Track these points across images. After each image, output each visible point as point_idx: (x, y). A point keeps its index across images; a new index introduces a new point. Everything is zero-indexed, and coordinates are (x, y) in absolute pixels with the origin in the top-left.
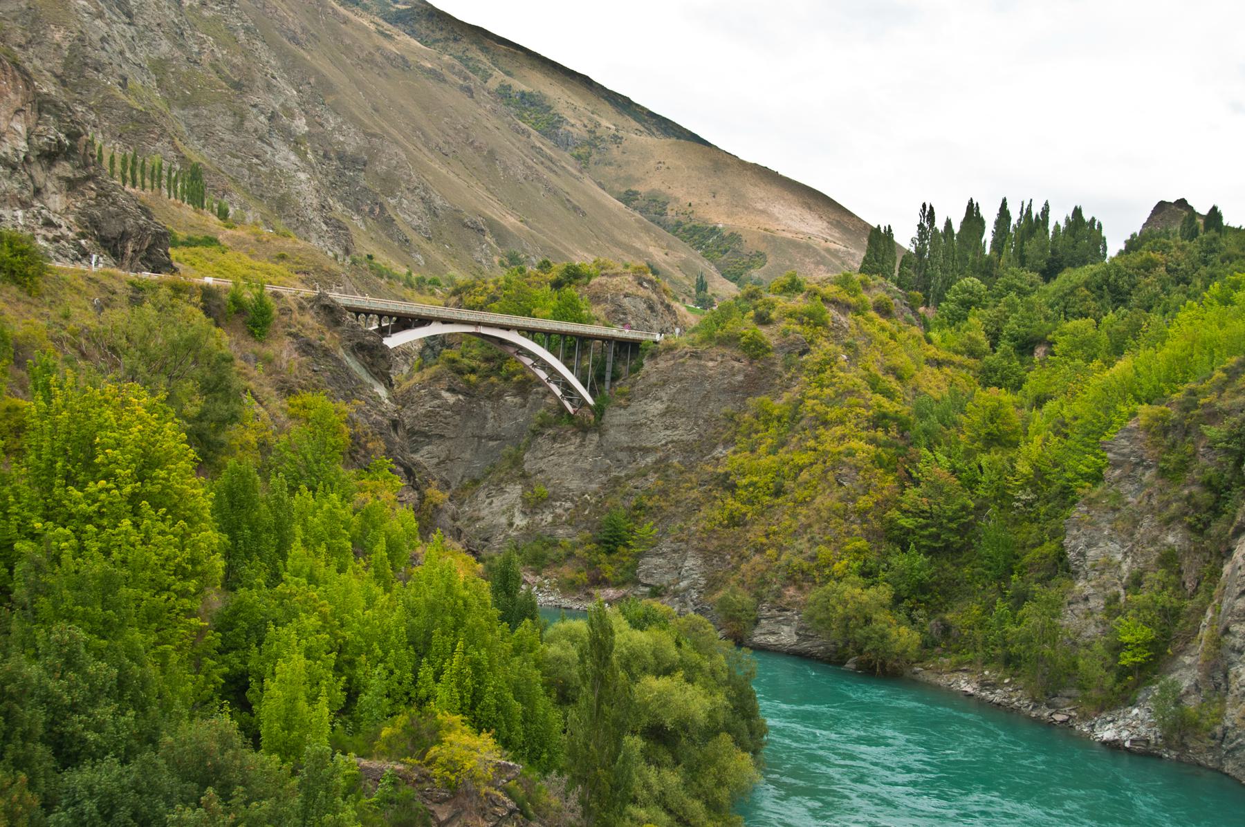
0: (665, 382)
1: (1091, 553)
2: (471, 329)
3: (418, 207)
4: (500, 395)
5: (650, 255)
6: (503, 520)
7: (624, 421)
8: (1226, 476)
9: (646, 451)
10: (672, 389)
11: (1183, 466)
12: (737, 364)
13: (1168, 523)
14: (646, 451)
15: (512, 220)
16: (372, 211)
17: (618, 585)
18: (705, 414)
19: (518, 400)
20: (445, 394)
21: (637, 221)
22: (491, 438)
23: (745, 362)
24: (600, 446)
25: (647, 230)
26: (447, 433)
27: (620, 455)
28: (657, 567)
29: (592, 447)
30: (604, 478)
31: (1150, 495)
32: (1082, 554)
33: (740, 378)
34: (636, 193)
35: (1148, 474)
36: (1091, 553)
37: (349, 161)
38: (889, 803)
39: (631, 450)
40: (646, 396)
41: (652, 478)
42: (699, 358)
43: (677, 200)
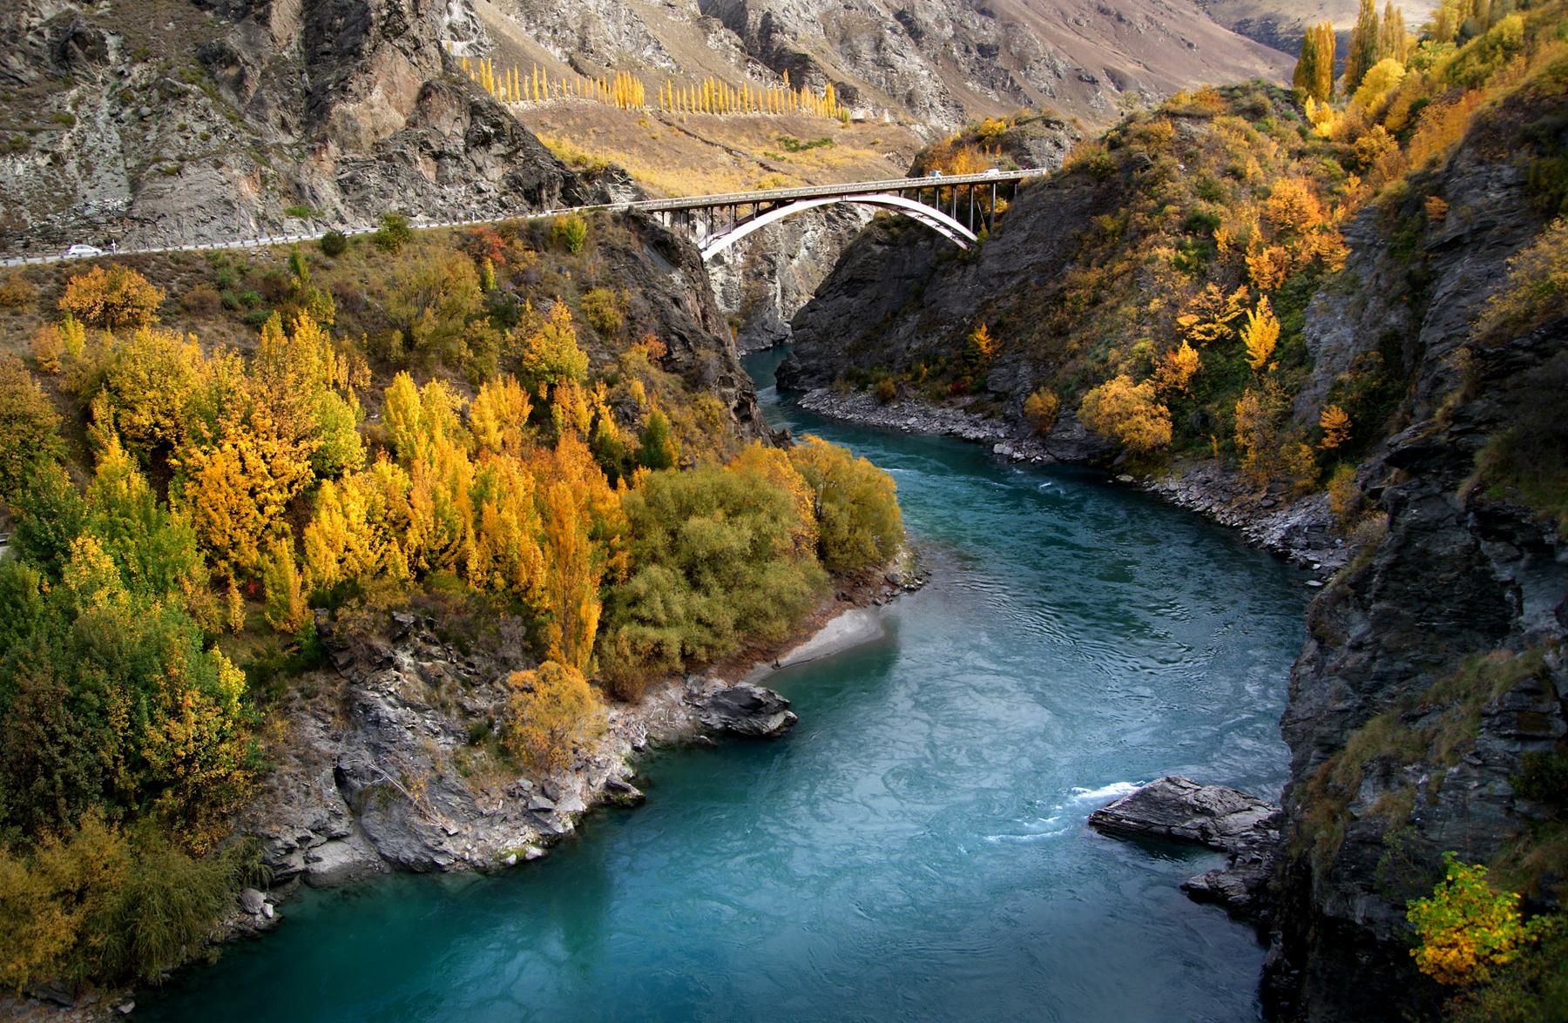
0: (1027, 213)
1: (1325, 339)
2: (838, 200)
3: (1048, 73)
4: (915, 242)
5: (1256, 72)
6: (904, 345)
7: (997, 250)
8: (1266, 270)
9: (1012, 275)
10: (1033, 218)
11: (1410, 244)
12: (1087, 188)
13: (1391, 304)
14: (1012, 275)
15: (1132, 66)
16: (1004, 85)
17: (973, 393)
18: (1058, 237)
19: (927, 243)
20: (874, 247)
21: (1246, 45)
22: (907, 278)
23: (1094, 185)
24: (976, 276)
25: (1255, 51)
26: (876, 278)
27: (992, 281)
28: (1001, 376)
29: (970, 277)
30: (979, 302)
31: (1378, 277)
32: (1317, 341)
33: (1089, 200)
34: (1248, 21)
35: (1381, 254)
36: (1325, 339)
37: (985, 51)
38: (699, 621)
39: (1000, 275)
40: (1013, 228)
41: (1014, 299)
42: (1056, 188)
43: (1287, 18)
